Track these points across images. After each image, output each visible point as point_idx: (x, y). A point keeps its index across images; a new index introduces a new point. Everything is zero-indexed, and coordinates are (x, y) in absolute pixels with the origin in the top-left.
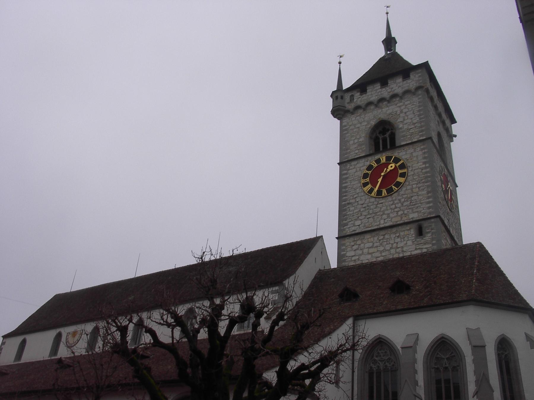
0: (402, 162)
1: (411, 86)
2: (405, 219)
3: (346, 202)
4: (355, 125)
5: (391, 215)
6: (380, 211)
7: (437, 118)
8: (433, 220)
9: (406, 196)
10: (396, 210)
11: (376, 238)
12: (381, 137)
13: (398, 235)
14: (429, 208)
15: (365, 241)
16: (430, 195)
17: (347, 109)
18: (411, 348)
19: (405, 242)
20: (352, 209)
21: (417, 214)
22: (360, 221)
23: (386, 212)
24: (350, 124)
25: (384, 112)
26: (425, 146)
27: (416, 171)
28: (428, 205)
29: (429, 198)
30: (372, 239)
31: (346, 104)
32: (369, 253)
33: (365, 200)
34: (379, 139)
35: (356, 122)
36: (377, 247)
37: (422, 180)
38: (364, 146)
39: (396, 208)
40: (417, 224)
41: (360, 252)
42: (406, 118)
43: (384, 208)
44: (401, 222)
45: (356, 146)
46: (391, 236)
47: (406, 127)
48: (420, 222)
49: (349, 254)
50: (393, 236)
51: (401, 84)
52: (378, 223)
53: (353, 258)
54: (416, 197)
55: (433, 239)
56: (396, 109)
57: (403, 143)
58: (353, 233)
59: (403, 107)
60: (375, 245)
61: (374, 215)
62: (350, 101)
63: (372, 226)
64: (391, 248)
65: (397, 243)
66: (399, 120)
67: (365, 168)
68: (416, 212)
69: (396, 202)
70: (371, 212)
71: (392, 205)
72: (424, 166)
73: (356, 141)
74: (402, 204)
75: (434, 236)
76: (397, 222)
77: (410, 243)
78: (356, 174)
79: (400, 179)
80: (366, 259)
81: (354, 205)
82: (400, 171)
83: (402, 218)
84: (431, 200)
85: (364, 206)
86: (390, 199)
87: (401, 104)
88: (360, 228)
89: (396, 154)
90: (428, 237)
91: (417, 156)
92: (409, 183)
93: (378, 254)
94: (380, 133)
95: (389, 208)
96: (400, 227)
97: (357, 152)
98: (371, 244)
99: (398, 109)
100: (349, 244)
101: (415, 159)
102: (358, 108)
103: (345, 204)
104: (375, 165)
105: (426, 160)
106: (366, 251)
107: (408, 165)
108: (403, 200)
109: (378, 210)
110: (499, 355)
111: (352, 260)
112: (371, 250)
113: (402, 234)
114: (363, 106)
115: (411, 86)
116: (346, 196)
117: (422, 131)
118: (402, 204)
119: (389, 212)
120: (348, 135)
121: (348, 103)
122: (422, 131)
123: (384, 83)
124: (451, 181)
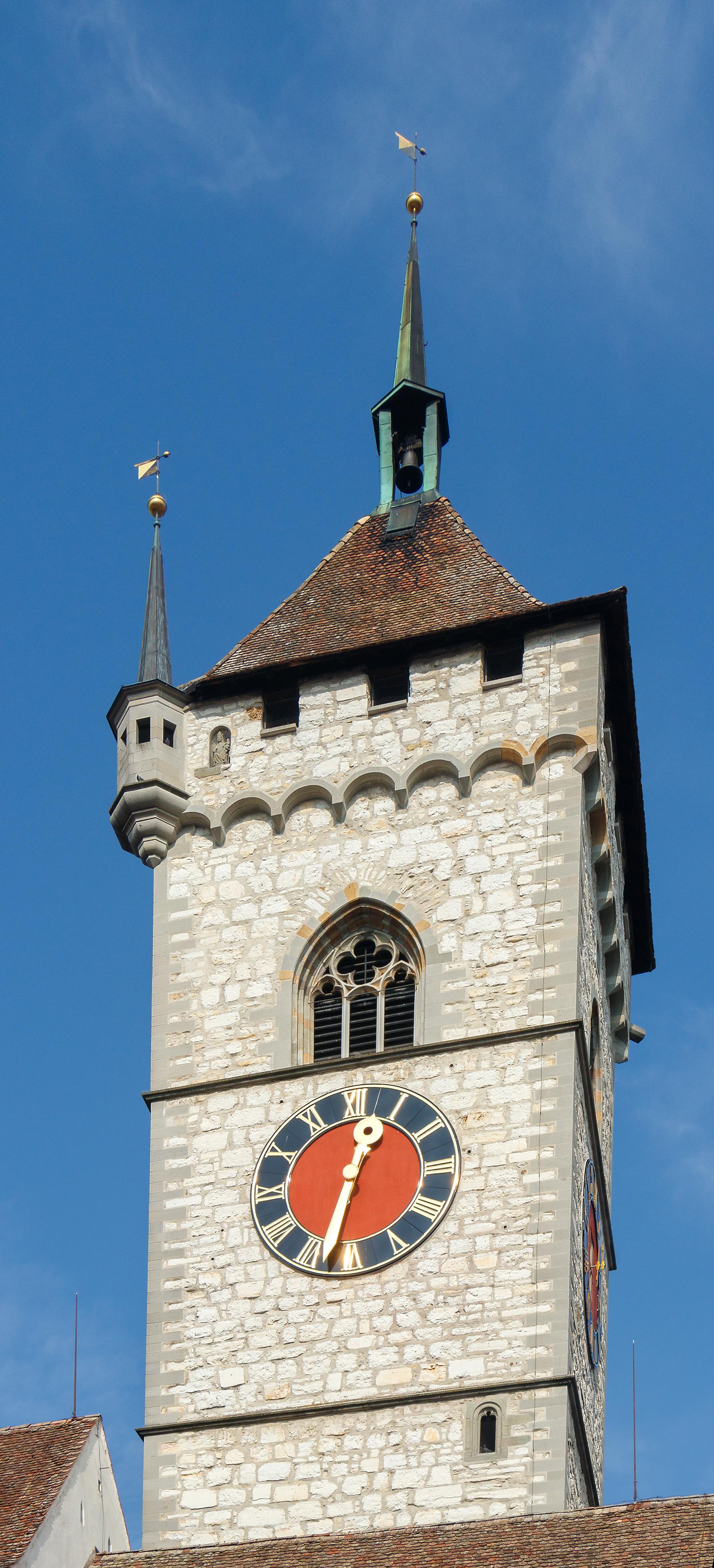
1: (522, 727)
3: (182, 1283)
4: (229, 906)
5: (376, 1358)
6: (327, 1336)
8: (542, 1393)
9: (443, 1281)
10: (395, 1337)
11: (305, 1448)
12: (348, 986)
13: (395, 1439)
14: (534, 1341)
15: (261, 1454)
16: (543, 1286)
17: (190, 806)
19: (424, 1471)
20: (206, 1313)
21: (479, 1361)
22: (240, 1371)
23: (353, 1343)
24: (207, 895)
25: (371, 855)
26: (547, 1063)
27: (495, 1174)
28: (531, 1331)
29: (536, 1298)
30: (289, 1449)
32: (273, 1503)
33: (267, 1281)
34: (338, 994)
35: (232, 890)
36: (308, 1480)
37: (515, 1219)
38: (269, 1025)
39: (396, 1327)
40: (479, 1400)
41: (239, 1496)
42: (477, 905)
45: (231, 1018)
47: (471, 951)
48: (489, 1398)
49: (189, 1500)
50: (376, 1441)
51: (474, 706)
52: (317, 1386)
53: (211, 1518)
54: (484, 1293)
55: (533, 1468)
57: (451, 1035)
59: (466, 845)
60: (304, 1471)
61: (301, 1349)
62: (212, 763)
63: (291, 1395)
64: (368, 1490)
65: (392, 1472)
66: (442, 913)
67: (270, 1132)
68: (478, 1354)
69: (396, 1303)
70: (289, 1334)
71: (381, 1312)
72: (532, 1155)
73: (233, 992)
74: (424, 1315)
75: (539, 1457)
76: (395, 1387)
77: (442, 1474)
78: (230, 1158)
80: (260, 1524)
81: (216, 1297)
83: (416, 1372)
84: (544, 1308)
85: (260, 1306)
86: (376, 1290)
87: (461, 824)
88: (238, 1399)
89: (412, 1077)
90: (515, 1458)
92: (461, 1226)
93: (312, 1509)
94: (345, 965)
95: (365, 1327)
96: (407, 1409)
97: (235, 1047)
99: (441, 850)
100: (191, 1459)
101: (497, 1117)
102: (248, 809)
103: (177, 1292)
105: (543, 1130)
106: (261, 1492)
108: (427, 1298)
109: (318, 1329)
111: (202, 1525)
112: (283, 1493)
113: (414, 1436)
114: (400, 777)
115: (522, 727)
116: (180, 1253)
117: (541, 986)
118: (424, 1315)
119: (366, 1342)
120: (191, 955)
121: (200, 774)
122: (541, 986)
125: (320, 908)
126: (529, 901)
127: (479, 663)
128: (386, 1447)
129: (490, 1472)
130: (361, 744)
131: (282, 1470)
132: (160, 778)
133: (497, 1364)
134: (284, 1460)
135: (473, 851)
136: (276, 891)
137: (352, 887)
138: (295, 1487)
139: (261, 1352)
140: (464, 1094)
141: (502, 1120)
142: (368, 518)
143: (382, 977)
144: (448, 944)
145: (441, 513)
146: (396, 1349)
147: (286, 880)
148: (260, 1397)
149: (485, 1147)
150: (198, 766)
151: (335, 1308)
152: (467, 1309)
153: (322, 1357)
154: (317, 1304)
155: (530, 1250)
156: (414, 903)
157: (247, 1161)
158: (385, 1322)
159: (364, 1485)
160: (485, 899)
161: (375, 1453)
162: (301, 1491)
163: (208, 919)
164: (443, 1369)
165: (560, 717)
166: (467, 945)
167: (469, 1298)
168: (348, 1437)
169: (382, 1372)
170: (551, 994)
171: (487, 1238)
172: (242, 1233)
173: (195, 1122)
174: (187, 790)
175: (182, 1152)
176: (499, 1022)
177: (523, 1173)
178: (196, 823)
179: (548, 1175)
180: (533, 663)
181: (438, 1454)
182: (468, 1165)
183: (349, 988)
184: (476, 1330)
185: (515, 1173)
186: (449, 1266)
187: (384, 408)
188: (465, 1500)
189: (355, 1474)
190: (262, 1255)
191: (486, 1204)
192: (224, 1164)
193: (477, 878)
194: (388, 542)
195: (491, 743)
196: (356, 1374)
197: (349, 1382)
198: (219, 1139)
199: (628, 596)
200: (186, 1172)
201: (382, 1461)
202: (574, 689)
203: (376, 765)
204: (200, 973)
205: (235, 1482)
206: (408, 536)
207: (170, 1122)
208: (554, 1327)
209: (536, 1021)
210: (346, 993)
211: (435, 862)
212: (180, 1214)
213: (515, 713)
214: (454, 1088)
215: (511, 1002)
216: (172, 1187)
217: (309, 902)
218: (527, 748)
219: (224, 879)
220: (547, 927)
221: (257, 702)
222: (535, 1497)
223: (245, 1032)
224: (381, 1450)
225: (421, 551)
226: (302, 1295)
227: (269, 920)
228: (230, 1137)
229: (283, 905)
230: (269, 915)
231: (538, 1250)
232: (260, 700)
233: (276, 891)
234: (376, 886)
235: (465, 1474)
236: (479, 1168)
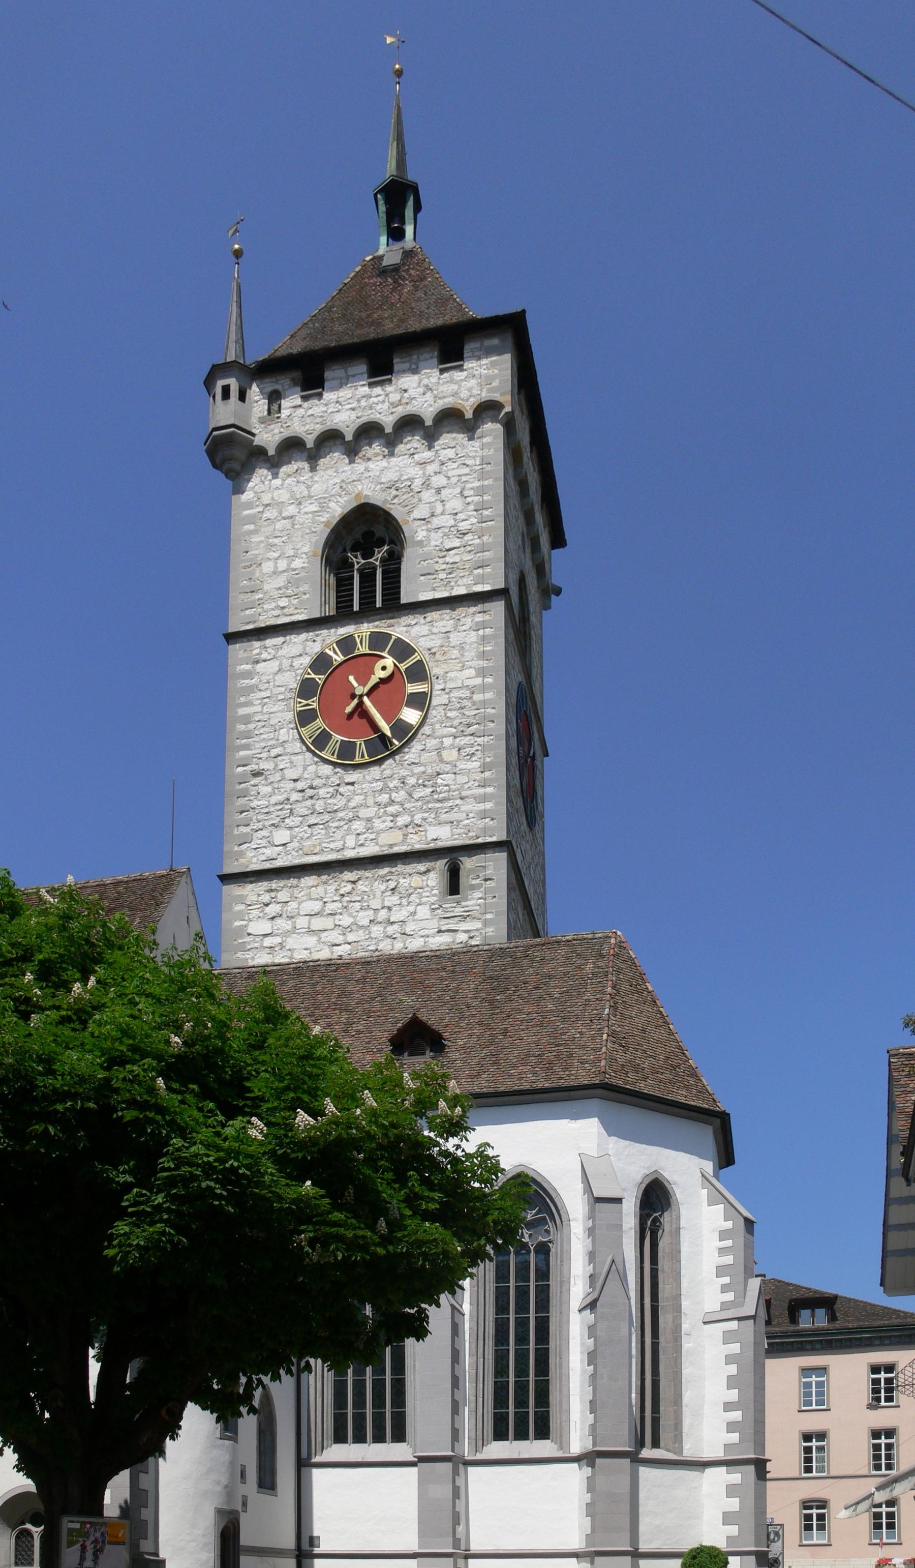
4: (280, 505)
5: (378, 824)
9: (422, 769)
10: (391, 809)
11: (331, 888)
14: (483, 815)
24: (266, 499)
28: (481, 806)
32: (311, 932)
33: (305, 768)
37: (469, 725)
39: (392, 802)
42: (439, 508)
47: (436, 539)
52: (339, 844)
53: (268, 942)
59: (431, 469)
60: (331, 907)
61: (327, 817)
65: (390, 909)
66: (416, 514)
67: (306, 661)
72: (479, 681)
73: (282, 565)
76: (391, 846)
77: (423, 912)
78: (280, 679)
84: (489, 790)
85: (300, 785)
89: (401, 629)
90: (473, 900)
93: (335, 936)
95: (370, 802)
97: (283, 602)
99: (414, 471)
101: (455, 653)
108: (412, 781)
109: (339, 802)
112: (317, 923)
116: (247, 747)
119: (370, 812)
120: (256, 539)
121: (262, 421)
125: (338, 509)
126: (472, 507)
127: (436, 353)
128: (385, 891)
129: (456, 910)
130: (363, 403)
131: (316, 906)
132: (237, 423)
133: (458, 831)
134: (317, 899)
135: (436, 473)
136: (310, 497)
137: (358, 495)
138: (324, 919)
139: (301, 819)
140: (433, 637)
141: (459, 656)
142: (371, 257)
143: (377, 559)
144: (421, 535)
145: (416, 255)
146: (392, 818)
147: (317, 489)
148: (301, 852)
149: (448, 675)
150: (261, 415)
151: (349, 787)
152: (438, 790)
153: (342, 823)
154: (339, 785)
155: (479, 748)
156: (400, 508)
157: (292, 681)
158: (384, 798)
159: (372, 918)
160: (444, 505)
161: (379, 894)
162: (328, 923)
163: (267, 515)
164: (423, 833)
165: (488, 389)
166: (433, 534)
167: (439, 781)
168: (360, 882)
169: (382, 835)
170: (488, 570)
171: (451, 738)
172: (288, 734)
173: (258, 654)
174: (254, 431)
175: (249, 675)
176: (455, 588)
177: (473, 693)
178: (260, 452)
179: (489, 695)
180: (470, 354)
181: (421, 897)
182: (437, 687)
183: (358, 563)
184: (445, 805)
185: (468, 693)
186: (425, 757)
187: (380, 191)
188: (440, 931)
189: (365, 909)
190: (301, 748)
191: (449, 714)
192: (277, 684)
193: (438, 491)
194: (384, 272)
195: (446, 404)
196: (365, 836)
197: (360, 842)
198: (274, 666)
199: (528, 316)
200: (252, 689)
201: (383, 900)
202: (496, 371)
203: (372, 416)
204: (262, 551)
205: (284, 915)
206: (395, 269)
207: (242, 654)
208: (497, 804)
209: (479, 588)
210: (356, 567)
211: (411, 479)
212: (247, 719)
213: (460, 386)
214: (426, 632)
215: (462, 574)
216: (242, 699)
217: (332, 504)
218: (468, 408)
219: (277, 488)
220: (484, 525)
221: (297, 374)
222: (487, 930)
223: (289, 592)
224: (383, 892)
225: (404, 279)
226: (328, 778)
227: (306, 516)
228: (280, 664)
229: (314, 508)
230: (306, 513)
231: (484, 748)
232: (300, 373)
233: (310, 497)
234: (377, 498)
235: (439, 911)
236: (443, 690)
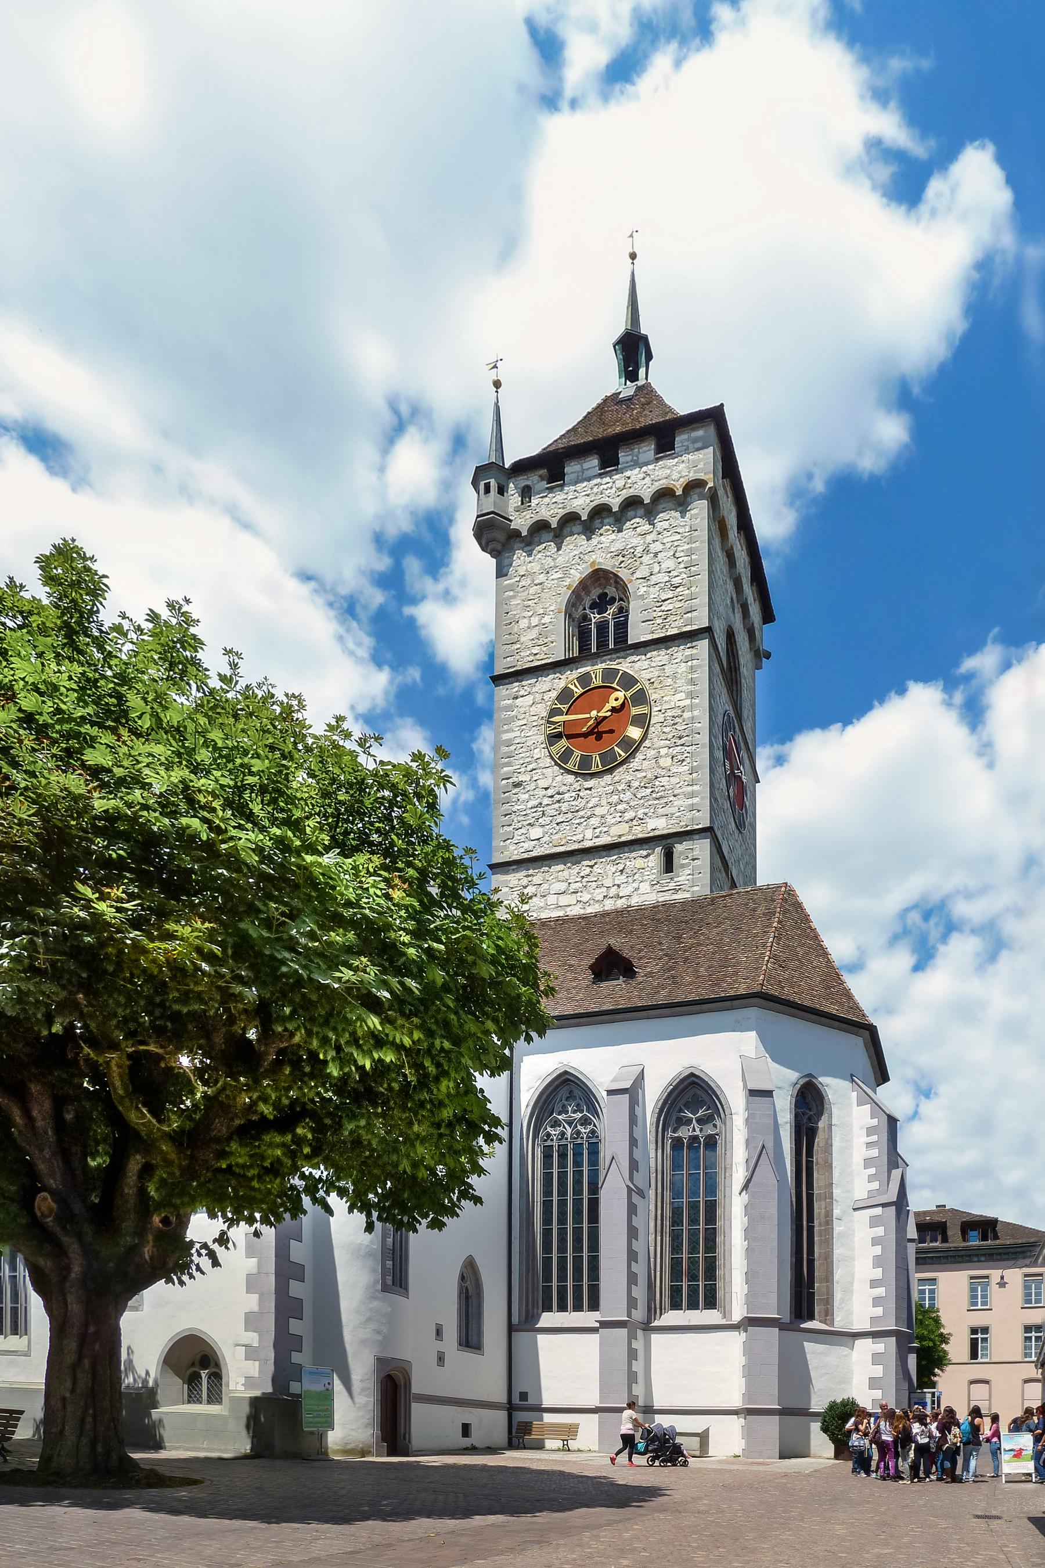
0: (638, 687)
2: (639, 833)
5: (610, 820)
7: (730, 587)
10: (620, 807)
18: (633, 1092)
21: (663, 820)
22: (541, 829)
31: (511, 509)
43: (594, 801)
44: (630, 838)
45: (534, 634)
46: (606, 868)
47: (654, 592)
52: (580, 837)
56: (635, 541)
58: (525, 856)
60: (574, 886)
65: (619, 886)
67: (554, 694)
72: (688, 702)
76: (620, 836)
79: (634, 733)
82: (635, 711)
85: (550, 792)
89: (626, 665)
91: (674, 676)
95: (604, 802)
98: (563, 886)
102: (540, 527)
104: (578, 690)
107: (654, 697)
108: (636, 784)
110: (796, 1116)
120: (514, 602)
123: (609, 462)
124: (747, 762)
